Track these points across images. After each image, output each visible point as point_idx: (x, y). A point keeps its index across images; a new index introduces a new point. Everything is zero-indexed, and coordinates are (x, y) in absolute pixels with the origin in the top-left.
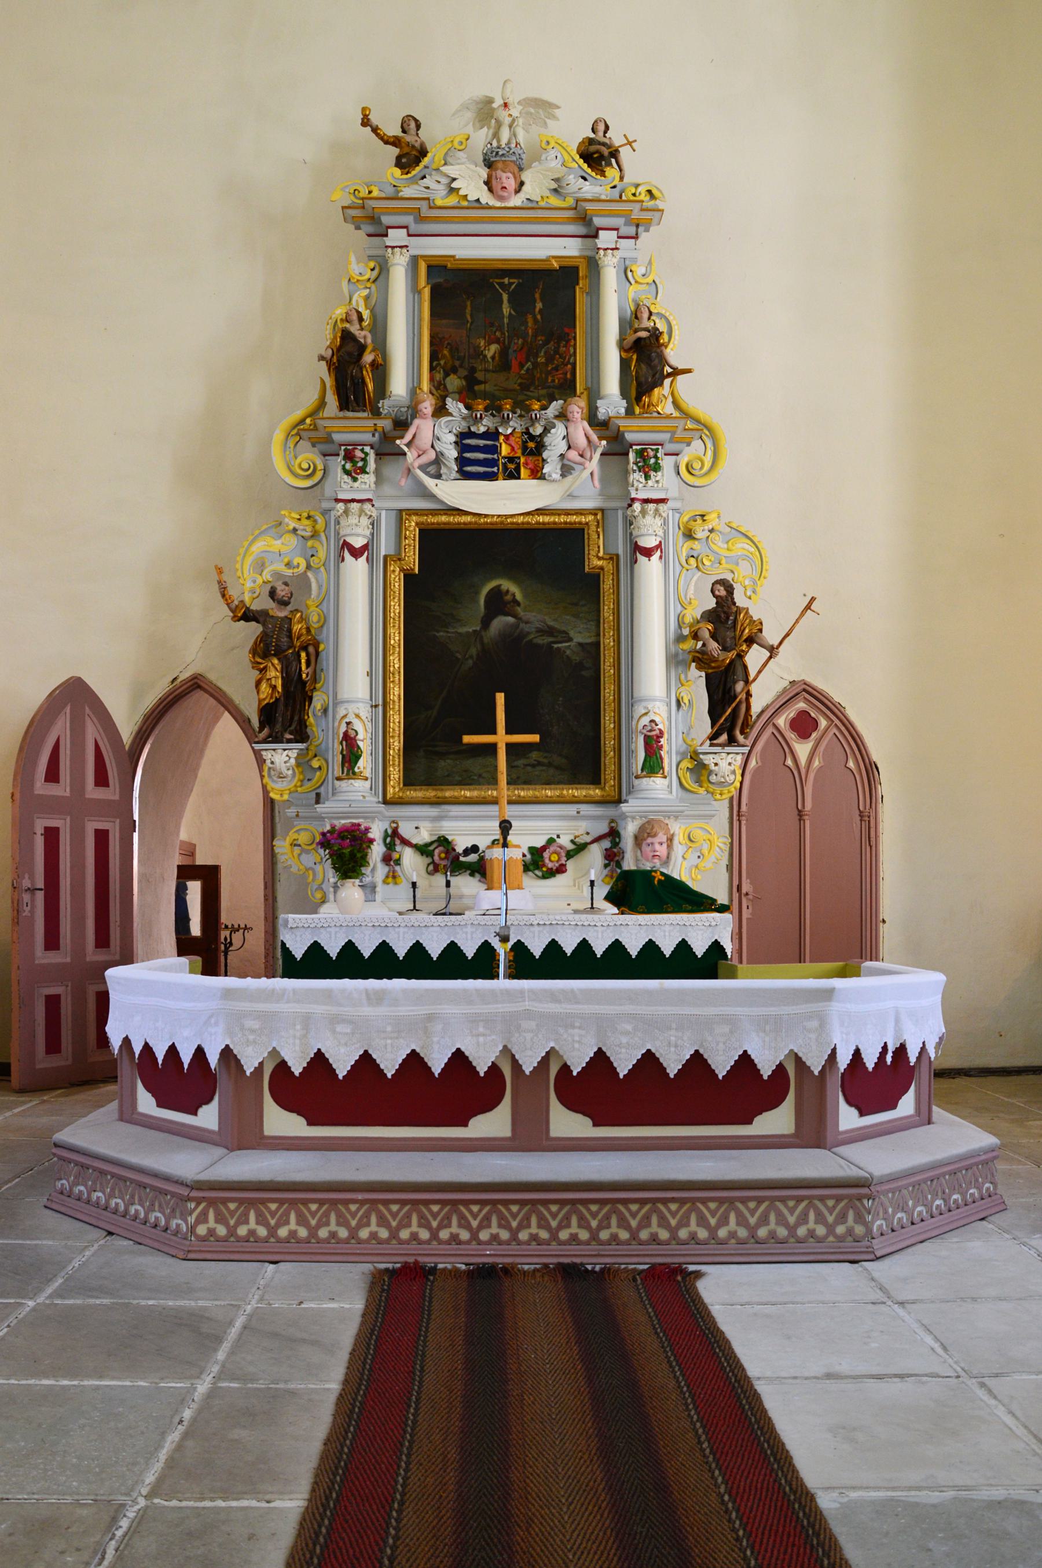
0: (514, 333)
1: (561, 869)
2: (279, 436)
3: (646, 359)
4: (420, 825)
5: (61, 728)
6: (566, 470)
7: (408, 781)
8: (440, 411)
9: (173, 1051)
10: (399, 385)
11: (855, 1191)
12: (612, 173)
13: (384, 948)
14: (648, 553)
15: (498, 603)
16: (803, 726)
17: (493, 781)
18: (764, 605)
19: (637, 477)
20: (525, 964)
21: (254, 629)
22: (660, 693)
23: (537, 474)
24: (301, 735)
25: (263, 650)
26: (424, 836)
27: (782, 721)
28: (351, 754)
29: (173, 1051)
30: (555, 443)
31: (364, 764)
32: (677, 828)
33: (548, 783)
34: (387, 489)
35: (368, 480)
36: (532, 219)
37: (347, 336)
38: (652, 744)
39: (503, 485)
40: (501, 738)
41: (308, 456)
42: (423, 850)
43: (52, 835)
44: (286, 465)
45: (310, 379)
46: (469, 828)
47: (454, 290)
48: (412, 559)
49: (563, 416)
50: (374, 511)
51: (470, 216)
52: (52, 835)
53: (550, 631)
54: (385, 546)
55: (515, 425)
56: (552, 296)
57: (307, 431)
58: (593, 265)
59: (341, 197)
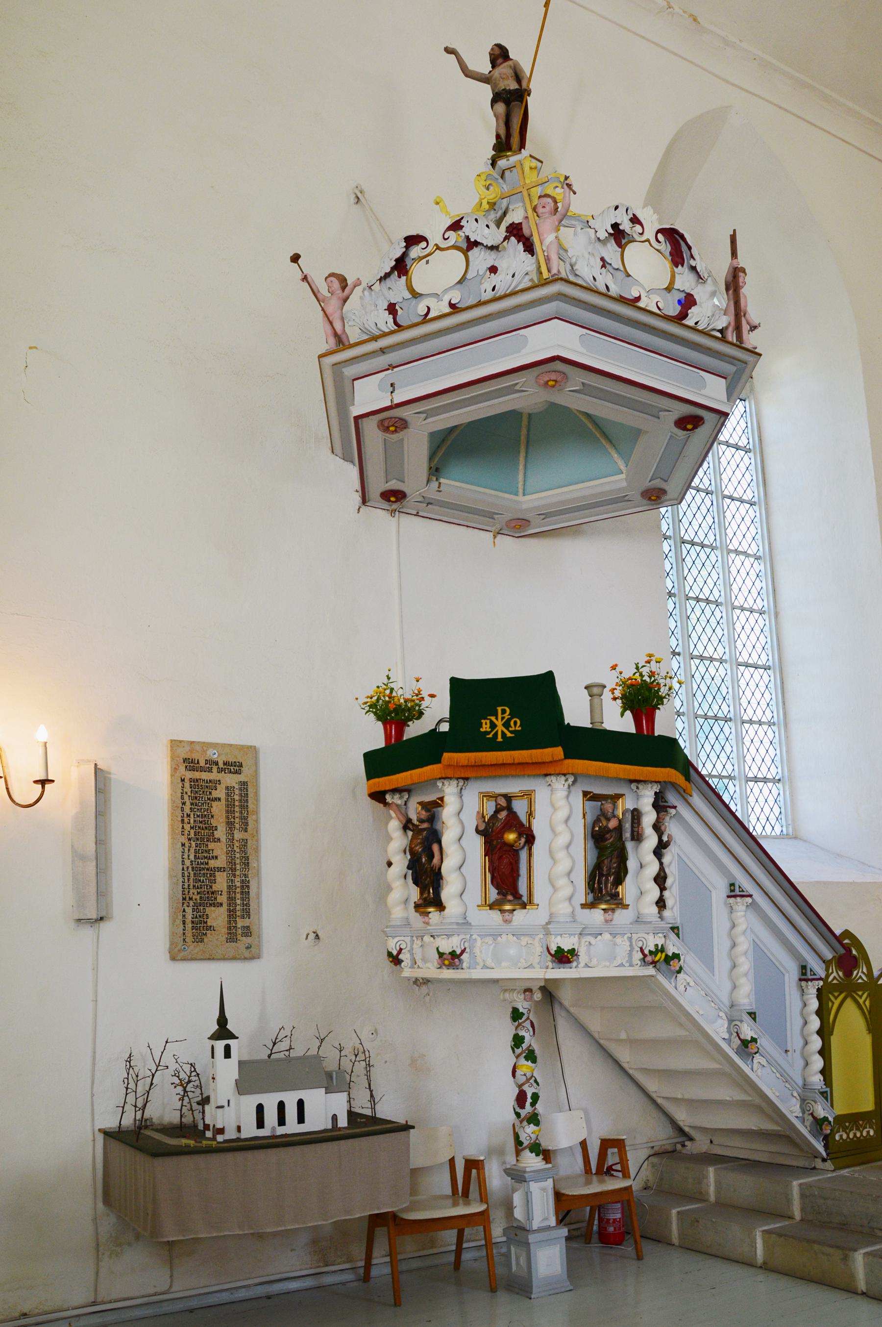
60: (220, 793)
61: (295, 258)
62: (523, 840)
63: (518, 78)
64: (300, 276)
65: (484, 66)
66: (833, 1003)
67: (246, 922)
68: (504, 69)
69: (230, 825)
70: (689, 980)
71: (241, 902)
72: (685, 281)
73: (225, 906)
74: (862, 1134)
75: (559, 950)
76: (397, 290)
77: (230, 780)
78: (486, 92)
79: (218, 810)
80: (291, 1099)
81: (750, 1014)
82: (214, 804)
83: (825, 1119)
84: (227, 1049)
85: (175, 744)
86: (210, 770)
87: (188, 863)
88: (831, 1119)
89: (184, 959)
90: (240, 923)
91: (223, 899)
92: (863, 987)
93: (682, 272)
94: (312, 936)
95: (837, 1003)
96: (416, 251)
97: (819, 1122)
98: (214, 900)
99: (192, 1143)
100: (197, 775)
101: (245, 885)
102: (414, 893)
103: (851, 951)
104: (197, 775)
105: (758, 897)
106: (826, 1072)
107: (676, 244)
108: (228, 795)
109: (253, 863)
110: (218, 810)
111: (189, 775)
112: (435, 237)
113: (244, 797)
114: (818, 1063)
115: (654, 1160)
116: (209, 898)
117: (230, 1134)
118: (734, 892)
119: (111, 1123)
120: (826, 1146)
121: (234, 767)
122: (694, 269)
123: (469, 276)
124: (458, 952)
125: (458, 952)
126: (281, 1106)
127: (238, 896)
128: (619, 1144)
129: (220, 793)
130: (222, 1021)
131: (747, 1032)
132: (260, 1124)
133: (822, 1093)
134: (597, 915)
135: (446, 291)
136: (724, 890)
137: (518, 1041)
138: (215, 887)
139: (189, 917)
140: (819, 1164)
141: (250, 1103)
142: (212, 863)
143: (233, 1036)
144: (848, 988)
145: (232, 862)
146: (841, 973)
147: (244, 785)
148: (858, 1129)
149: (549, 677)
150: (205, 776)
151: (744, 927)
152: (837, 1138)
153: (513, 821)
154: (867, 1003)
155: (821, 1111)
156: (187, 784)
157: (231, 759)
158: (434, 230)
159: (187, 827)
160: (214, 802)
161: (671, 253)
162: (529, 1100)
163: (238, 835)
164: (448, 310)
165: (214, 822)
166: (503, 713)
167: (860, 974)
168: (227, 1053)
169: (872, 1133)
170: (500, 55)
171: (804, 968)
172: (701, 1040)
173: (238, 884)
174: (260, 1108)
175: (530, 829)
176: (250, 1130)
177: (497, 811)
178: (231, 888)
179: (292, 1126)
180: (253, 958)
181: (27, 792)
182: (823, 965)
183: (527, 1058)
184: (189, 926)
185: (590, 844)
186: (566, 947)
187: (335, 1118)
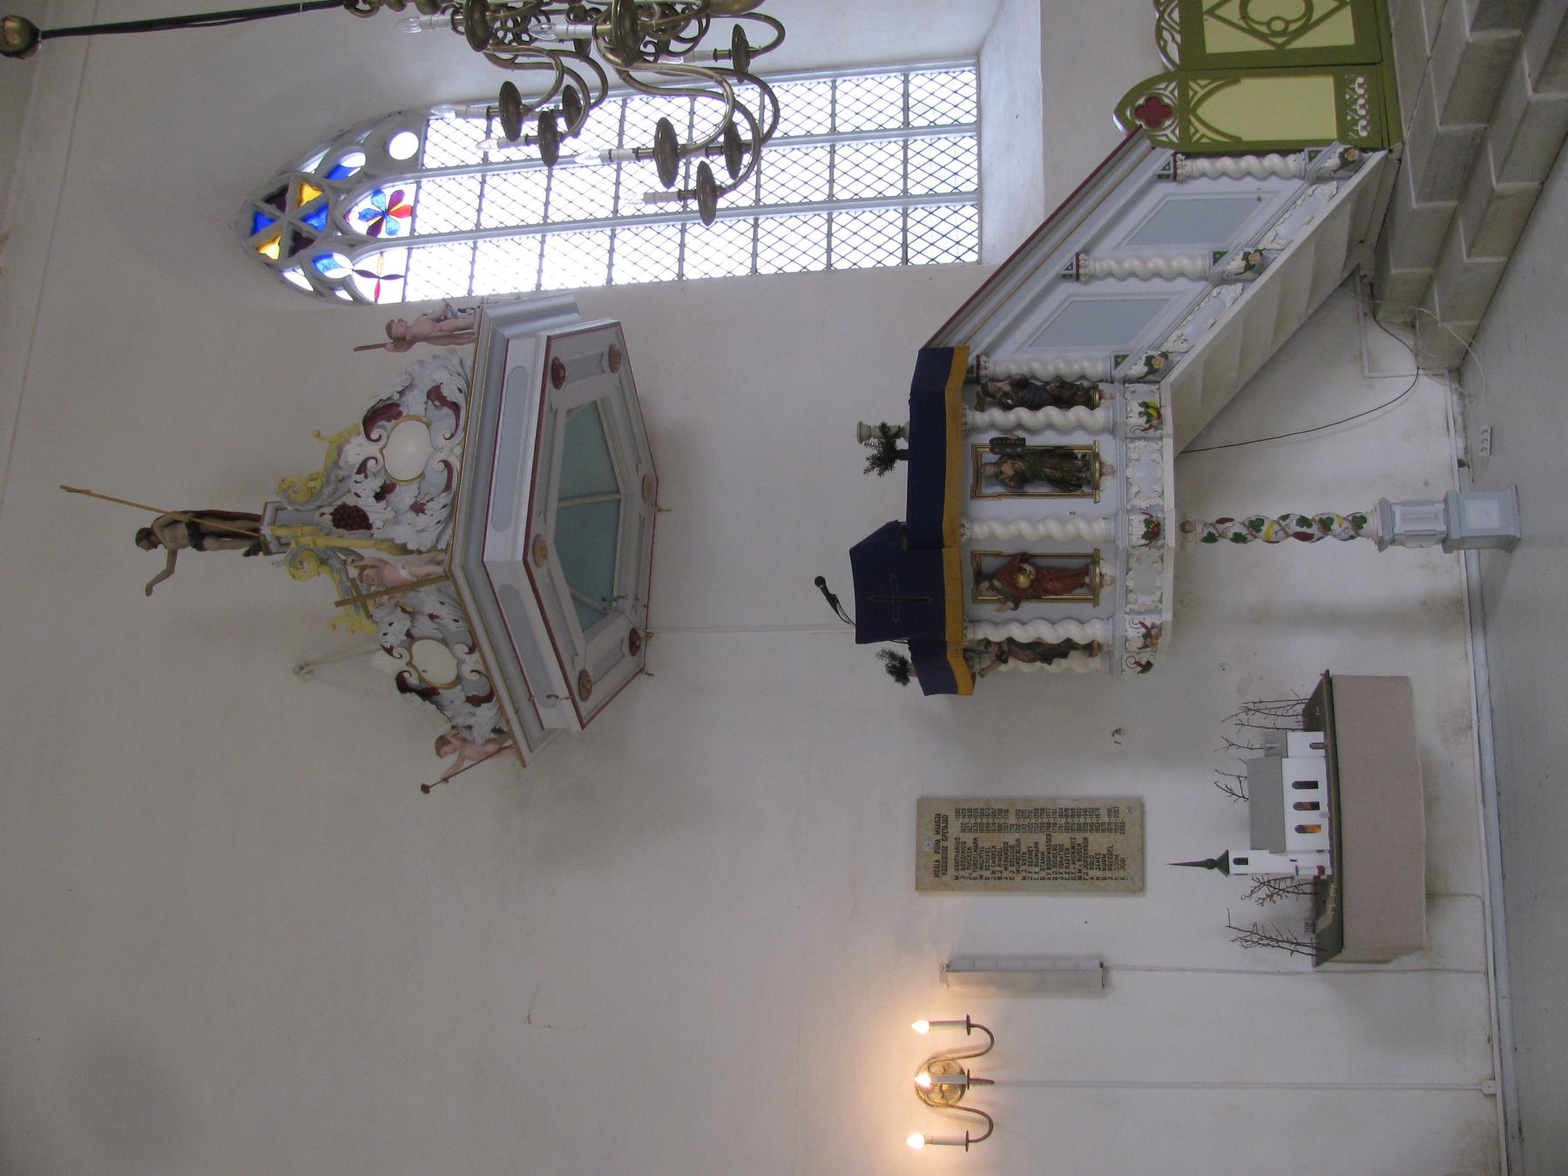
60: (968, 838)
61: (425, 789)
62: (1026, 566)
64: (443, 785)
65: (161, 553)
66: (1203, 136)
67: (1104, 813)
69: (1001, 828)
70: (1174, 337)
71: (1083, 817)
72: (415, 403)
73: (1087, 835)
74: (1362, 117)
75: (1145, 536)
77: (954, 828)
78: (187, 555)
79: (986, 841)
80: (1292, 796)
81: (1215, 261)
82: (980, 844)
83: (1342, 156)
84: (1239, 861)
85: (920, 886)
86: (945, 849)
87: (1043, 874)
88: (1341, 149)
89: (1143, 880)
90: (1104, 819)
91: (1079, 837)
92: (1183, 88)
94: (1117, 737)
95: (1203, 130)
96: (413, 680)
97: (1347, 165)
98: (1085, 849)
99: (1333, 886)
100: (951, 863)
101: (1065, 813)
103: (1141, 107)
104: (951, 863)
106: (1285, 149)
107: (382, 414)
108: (970, 830)
109: (1042, 805)
110: (986, 841)
111: (951, 870)
112: (400, 665)
113: (970, 812)
114: (1273, 160)
115: (1380, 315)
117: (1325, 860)
118: (1074, 274)
120: (1374, 150)
121: (941, 823)
122: (401, 393)
123: (439, 635)
124: (1143, 630)
125: (1143, 630)
126: (1299, 806)
127: (1076, 820)
129: (968, 838)
130: (1209, 864)
131: (1236, 264)
132: (1315, 829)
133: (1311, 159)
135: (455, 656)
137: (1239, 538)
138: (1067, 845)
139: (1099, 873)
140: (1396, 155)
141: (1293, 840)
142: (1042, 848)
143: (1226, 855)
144: (1186, 110)
145: (1041, 827)
146: (1167, 123)
148: (1355, 123)
150: (951, 855)
151: (1113, 263)
152: (1364, 134)
154: (1203, 82)
156: (962, 873)
157: (932, 826)
158: (391, 666)
159: (1005, 874)
160: (977, 846)
161: (389, 420)
162: (1305, 529)
163: (1012, 820)
164: (477, 655)
165: (1000, 845)
167: (1168, 94)
168: (1242, 861)
169: (1360, 80)
170: (147, 538)
171: (1161, 177)
173: (1063, 821)
174: (1301, 829)
175: (1013, 557)
176: (1322, 840)
177: (992, 588)
178: (1068, 828)
179: (1320, 795)
180: (1143, 813)
181: (978, 1038)
182: (1158, 150)
183: (1258, 530)
184: (1108, 873)
185: (1029, 489)
186: (1143, 529)
187: (1314, 746)
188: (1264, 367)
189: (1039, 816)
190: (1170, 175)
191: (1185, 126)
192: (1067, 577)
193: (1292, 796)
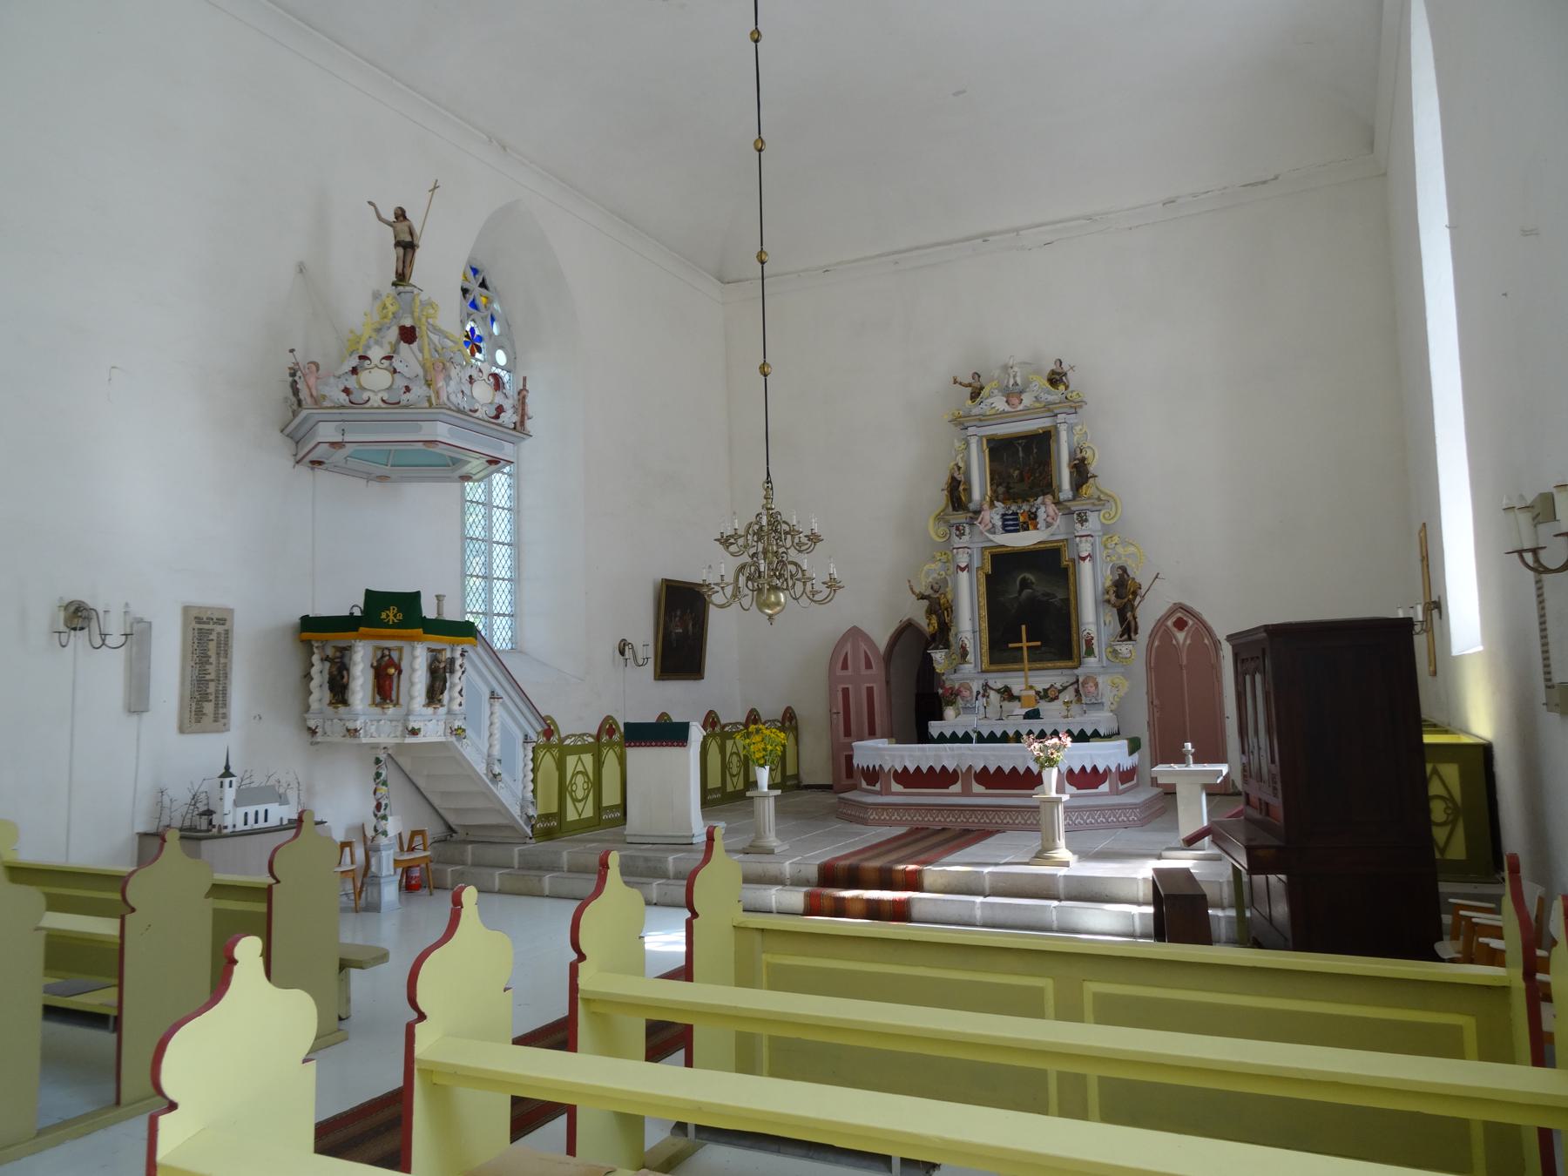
0: (1024, 465)
1: (1056, 698)
2: (931, 522)
3: (1081, 472)
4: (998, 681)
5: (848, 648)
6: (1049, 525)
7: (992, 662)
8: (992, 505)
9: (1083, 768)
10: (976, 495)
11: (865, 807)
12: (1062, 387)
13: (954, 734)
14: (1084, 559)
15: (1025, 584)
16: (1181, 624)
17: (1021, 660)
18: (1140, 575)
19: (1078, 526)
20: (981, 739)
21: (926, 603)
22: (1092, 616)
23: (1036, 528)
24: (947, 646)
25: (930, 612)
26: (999, 685)
27: (1170, 623)
28: (964, 653)
29: (1083, 768)
30: (1041, 515)
31: (970, 657)
32: (1100, 680)
33: (1050, 660)
34: (976, 539)
35: (966, 538)
36: (1028, 413)
37: (953, 478)
38: (1089, 643)
39: (1022, 534)
40: (1025, 644)
41: (943, 529)
42: (998, 691)
43: (846, 692)
44: (934, 532)
45: (941, 498)
46: (1017, 684)
47: (1000, 449)
48: (988, 569)
49: (1044, 503)
50: (972, 549)
51: (1001, 417)
52: (846, 692)
53: (1047, 594)
54: (976, 563)
55: (1026, 507)
56: (1041, 443)
57: (940, 518)
58: (1056, 427)
59: (947, 417)
63: (411, 234)
65: (392, 218)
68: (402, 226)
71: (222, 699)
76: (351, 382)
77: (219, 628)
80: (261, 809)
85: (186, 610)
91: (212, 697)
92: (555, 746)
93: (499, 393)
97: (530, 818)
98: (204, 700)
102: (327, 695)
105: (506, 698)
110: (212, 646)
116: (204, 697)
117: (230, 830)
118: (493, 696)
119: (142, 829)
121: (221, 621)
128: (422, 833)
130: (227, 767)
131: (497, 770)
134: (430, 710)
136: (487, 695)
137: (378, 775)
141: (241, 811)
144: (548, 747)
147: (227, 632)
149: (418, 594)
153: (392, 663)
155: (531, 812)
166: (393, 611)
167: (554, 739)
170: (401, 215)
172: (472, 775)
176: (240, 827)
179: (262, 824)
188: (418, 788)
189: (224, 675)
190: (526, 740)
191: (544, 746)
192: (339, 690)
193: (261, 809)
